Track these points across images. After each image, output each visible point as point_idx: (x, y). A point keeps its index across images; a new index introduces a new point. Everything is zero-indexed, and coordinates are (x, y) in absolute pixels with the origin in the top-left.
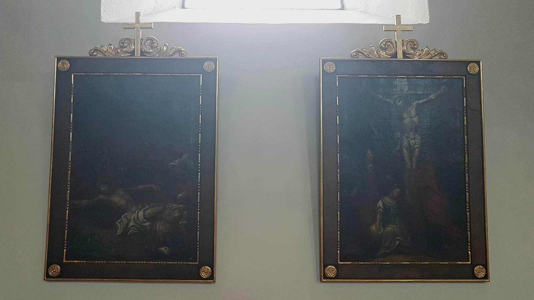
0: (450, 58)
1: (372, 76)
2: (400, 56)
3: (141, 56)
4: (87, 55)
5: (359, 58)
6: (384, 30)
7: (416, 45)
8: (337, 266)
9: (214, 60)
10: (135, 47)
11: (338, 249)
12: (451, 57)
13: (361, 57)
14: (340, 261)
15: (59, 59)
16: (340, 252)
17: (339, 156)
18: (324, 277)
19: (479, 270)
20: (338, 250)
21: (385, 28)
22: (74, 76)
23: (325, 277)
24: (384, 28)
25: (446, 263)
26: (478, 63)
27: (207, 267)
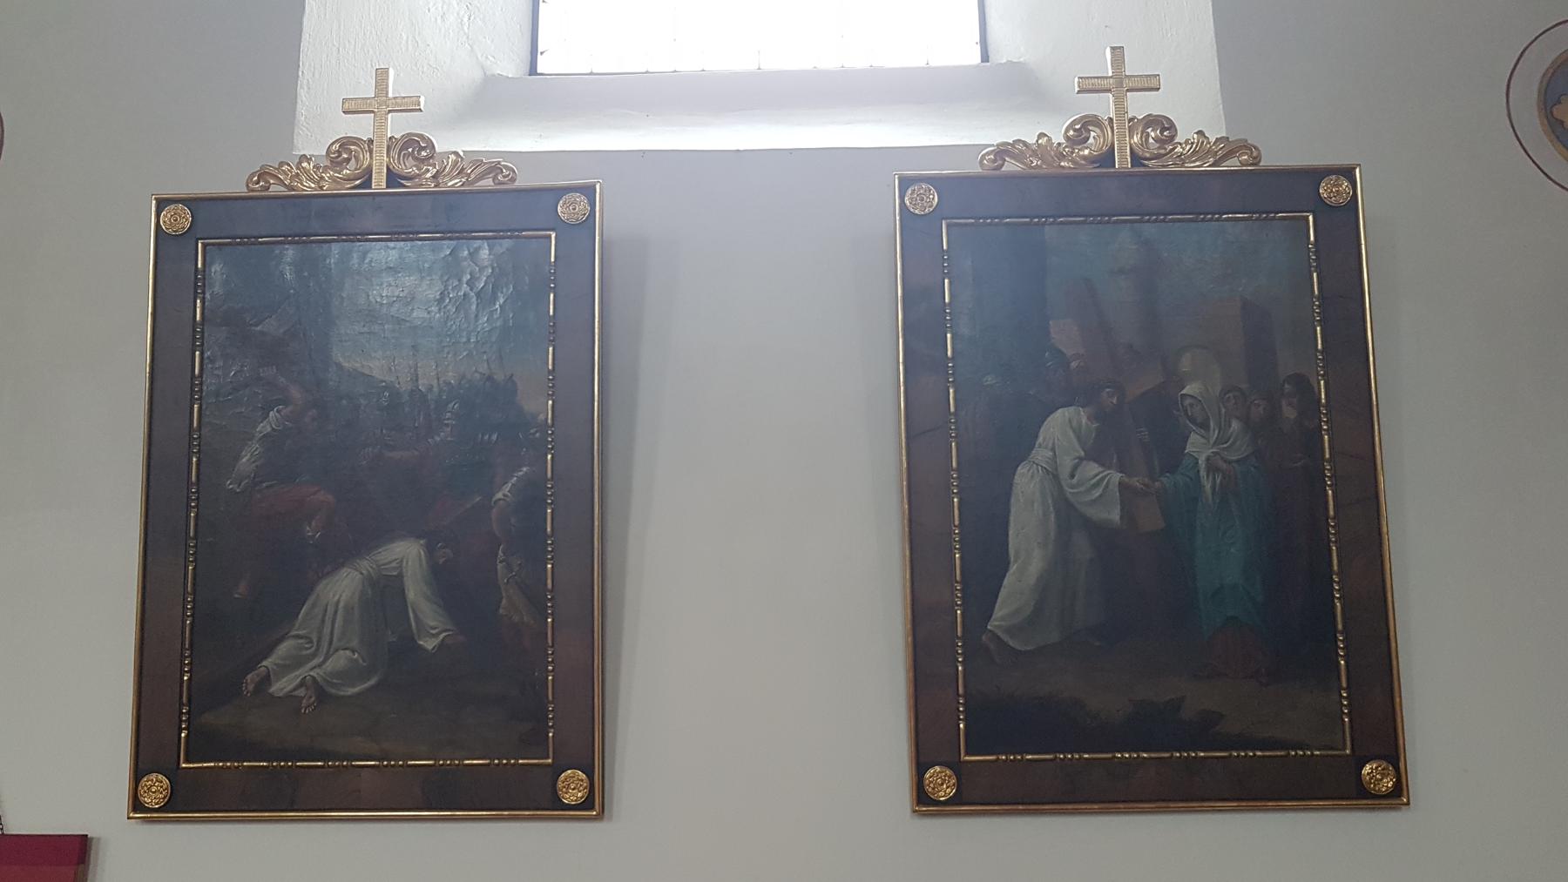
0: (1266, 162)
1: (981, 221)
2: (379, 183)
3: (388, 187)
4: (239, 189)
5: (1261, 164)
6: (1076, 91)
7: (424, 149)
8: (957, 767)
9: (588, 191)
10: (1127, 142)
11: (959, 716)
12: (1275, 156)
13: (1011, 166)
14: (187, 761)
15: (162, 204)
16: (965, 726)
17: (1329, 441)
18: (592, 805)
19: (572, 785)
20: (960, 719)
21: (1079, 86)
22: (948, 226)
23: (587, 804)
24: (1076, 85)
25: (373, 763)
26: (1348, 173)
27: (1367, 769)
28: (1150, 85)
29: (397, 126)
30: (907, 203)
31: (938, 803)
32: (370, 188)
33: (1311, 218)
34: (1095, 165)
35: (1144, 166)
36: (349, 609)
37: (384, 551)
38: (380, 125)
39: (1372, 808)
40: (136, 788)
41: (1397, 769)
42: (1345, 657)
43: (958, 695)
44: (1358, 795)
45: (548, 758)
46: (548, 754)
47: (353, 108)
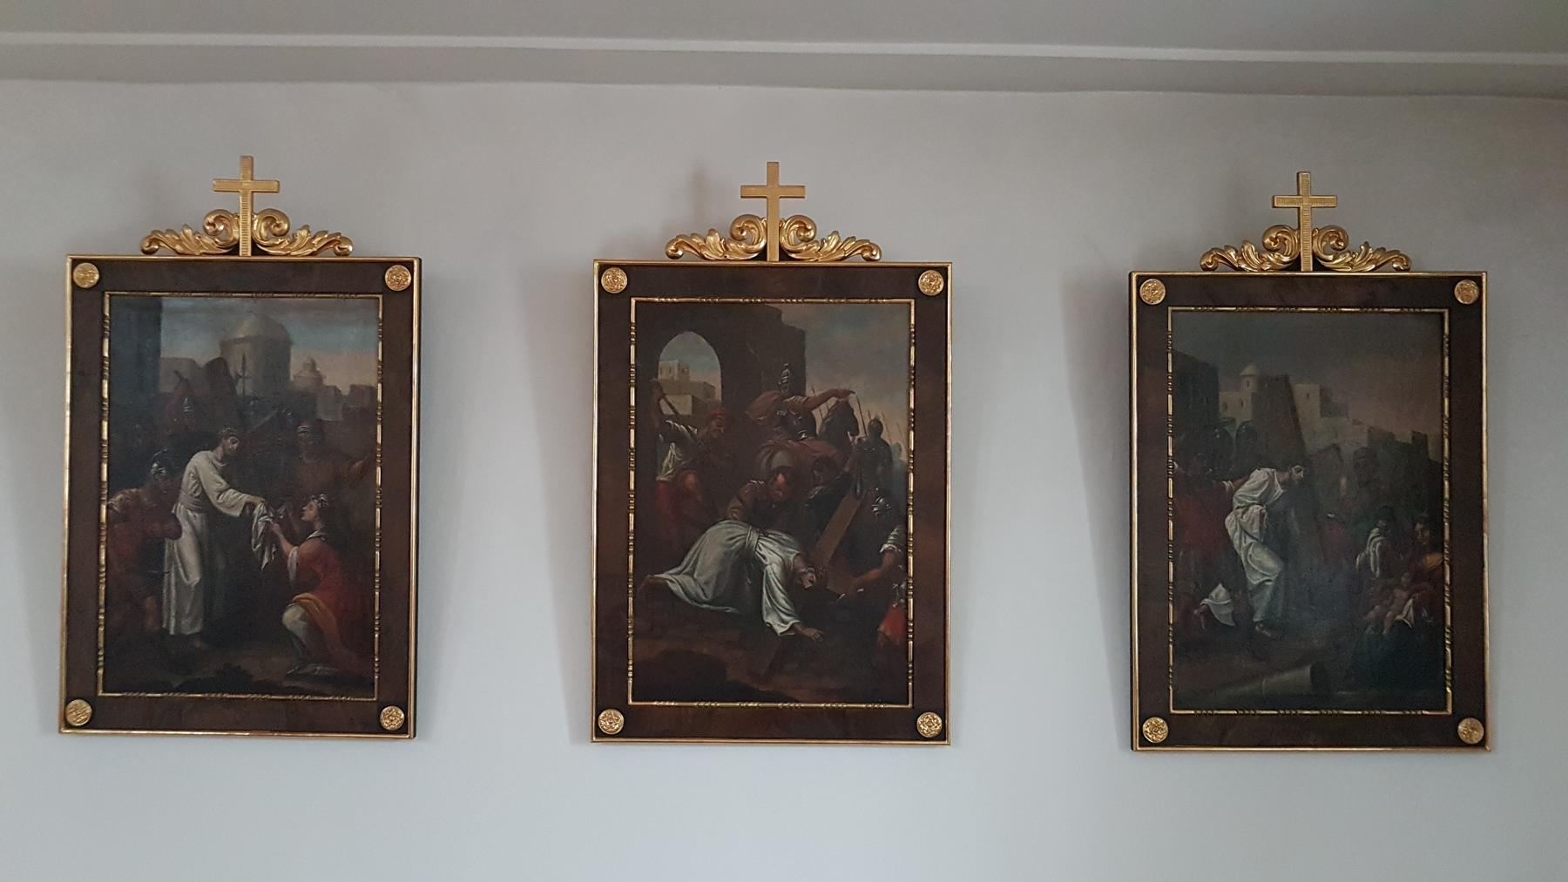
15: (75, 263)
28: (797, 193)
29: (788, 208)
30: (603, 284)
31: (406, 718)
32: (1299, 270)
33: (913, 303)
34: (224, 251)
35: (266, 254)
36: (196, 586)
37: (705, 554)
38: (772, 208)
39: (61, 706)
40: (65, 710)
41: (1484, 726)
42: (1451, 646)
43: (1169, 666)
44: (1453, 741)
45: (633, 700)
46: (374, 693)
47: (753, 192)
